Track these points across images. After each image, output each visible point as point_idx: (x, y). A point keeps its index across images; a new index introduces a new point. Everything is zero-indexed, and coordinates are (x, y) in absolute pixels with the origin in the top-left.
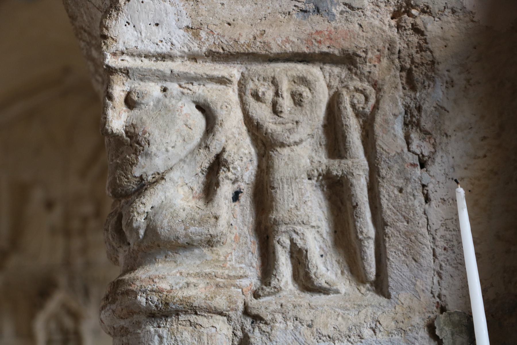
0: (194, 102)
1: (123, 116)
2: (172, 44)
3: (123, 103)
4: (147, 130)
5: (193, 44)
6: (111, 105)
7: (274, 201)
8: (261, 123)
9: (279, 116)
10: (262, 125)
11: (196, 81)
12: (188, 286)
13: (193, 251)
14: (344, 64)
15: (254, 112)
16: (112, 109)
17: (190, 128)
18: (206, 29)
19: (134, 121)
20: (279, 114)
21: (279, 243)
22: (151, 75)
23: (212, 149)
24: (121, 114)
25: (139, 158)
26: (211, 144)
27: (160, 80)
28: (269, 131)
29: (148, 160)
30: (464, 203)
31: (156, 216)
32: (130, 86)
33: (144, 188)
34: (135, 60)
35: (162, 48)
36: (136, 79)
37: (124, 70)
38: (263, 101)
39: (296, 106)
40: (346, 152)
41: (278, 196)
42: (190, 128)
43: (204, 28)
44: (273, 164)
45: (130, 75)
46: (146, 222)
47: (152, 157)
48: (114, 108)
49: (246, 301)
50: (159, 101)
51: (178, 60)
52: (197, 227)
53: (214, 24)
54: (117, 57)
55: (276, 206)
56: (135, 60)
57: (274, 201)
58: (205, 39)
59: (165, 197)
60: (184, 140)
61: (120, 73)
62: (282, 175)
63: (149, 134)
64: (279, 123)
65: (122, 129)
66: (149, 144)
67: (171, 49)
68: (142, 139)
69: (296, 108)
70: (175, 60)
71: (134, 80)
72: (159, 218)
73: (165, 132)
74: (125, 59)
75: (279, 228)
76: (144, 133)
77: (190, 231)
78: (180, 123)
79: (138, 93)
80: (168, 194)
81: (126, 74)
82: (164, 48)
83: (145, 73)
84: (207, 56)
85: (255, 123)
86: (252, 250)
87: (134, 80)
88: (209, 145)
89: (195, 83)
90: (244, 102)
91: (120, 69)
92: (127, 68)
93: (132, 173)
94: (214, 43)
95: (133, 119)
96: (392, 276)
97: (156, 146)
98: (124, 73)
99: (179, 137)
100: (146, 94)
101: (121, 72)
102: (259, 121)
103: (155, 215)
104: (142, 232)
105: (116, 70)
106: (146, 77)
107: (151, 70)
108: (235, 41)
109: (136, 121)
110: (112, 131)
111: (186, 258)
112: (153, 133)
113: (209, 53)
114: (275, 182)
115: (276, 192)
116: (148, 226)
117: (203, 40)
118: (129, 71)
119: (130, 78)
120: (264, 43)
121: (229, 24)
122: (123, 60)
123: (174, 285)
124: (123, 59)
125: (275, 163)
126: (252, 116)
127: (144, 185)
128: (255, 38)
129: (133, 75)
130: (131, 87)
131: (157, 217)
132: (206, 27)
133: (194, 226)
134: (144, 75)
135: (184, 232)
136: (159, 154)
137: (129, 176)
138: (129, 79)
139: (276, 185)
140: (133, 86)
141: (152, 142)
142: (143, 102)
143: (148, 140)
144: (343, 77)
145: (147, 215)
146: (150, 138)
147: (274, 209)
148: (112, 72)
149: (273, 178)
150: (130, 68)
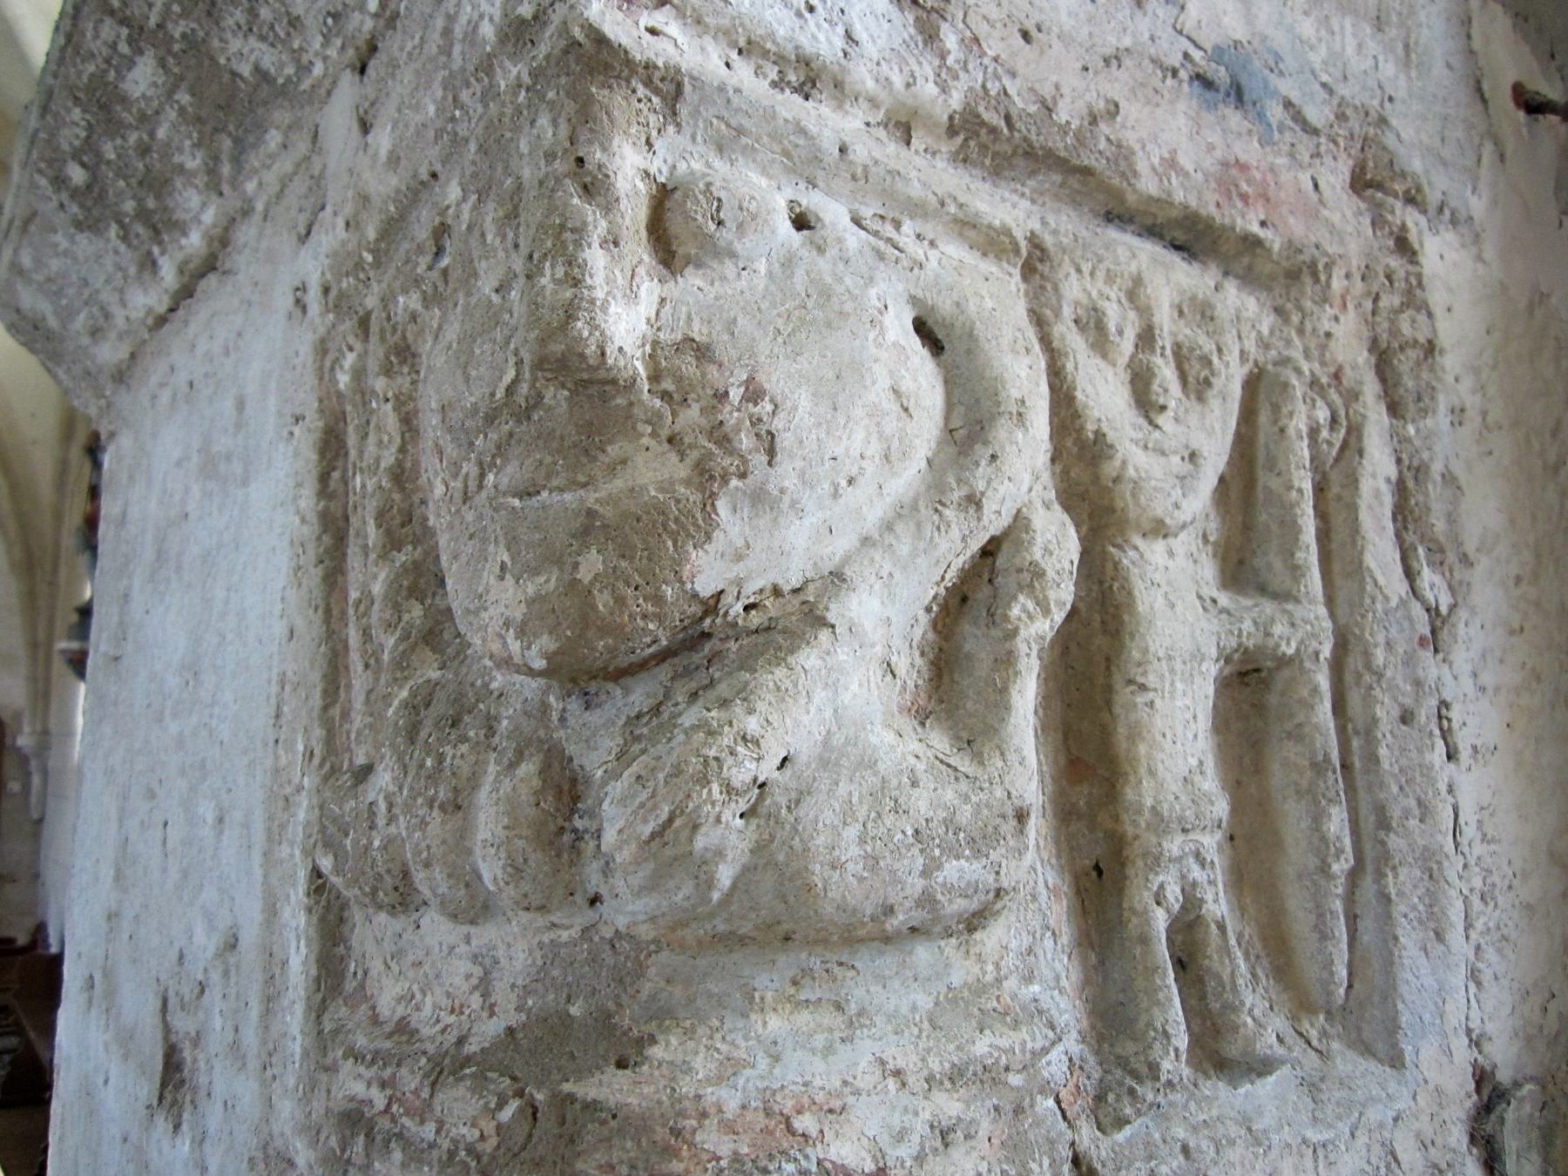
0: (914, 300)
1: (643, 293)
2: (849, 36)
3: (644, 234)
4: (767, 386)
5: (920, 63)
6: (603, 224)
7: (1143, 739)
8: (1111, 437)
9: (1151, 422)
10: (1111, 447)
11: (911, 219)
12: (946, 1145)
13: (911, 953)
14: (1269, 289)
15: (1089, 389)
16: (603, 244)
17: (906, 410)
18: (961, 26)
19: (696, 325)
20: (1152, 415)
21: (1158, 903)
22: (765, 139)
23: (989, 506)
24: (637, 279)
25: (722, 506)
26: (989, 493)
27: (790, 171)
28: (1131, 472)
29: (762, 522)
30: (1035, 664)
31: (803, 805)
32: (670, 161)
33: (708, 647)
34: (703, 49)
35: (814, 37)
36: (699, 138)
37: (662, 80)
38: (1110, 356)
39: (1188, 397)
40: (1298, 583)
41: (1159, 722)
42: (906, 410)
43: (953, 16)
44: (1130, 594)
45: (684, 110)
46: (753, 827)
47: (780, 511)
48: (616, 244)
49: (1081, 1149)
50: (789, 262)
51: (855, 110)
52: (968, 858)
53: (984, 17)
54: (633, 8)
55: (1149, 757)
56: (703, 49)
57: (1143, 739)
58: (957, 61)
59: (836, 711)
60: (887, 457)
61: (642, 91)
62: (1167, 642)
63: (772, 401)
64: (1154, 450)
65: (639, 354)
66: (771, 452)
67: (845, 54)
68: (740, 421)
69: (1188, 404)
70: (847, 106)
71: (694, 138)
72: (821, 813)
73: (835, 409)
74: (667, 30)
75: (1165, 844)
76: (754, 394)
77: (940, 880)
78: (878, 393)
79: (719, 200)
80: (846, 698)
81: (664, 99)
82: (821, 37)
83: (746, 123)
84: (952, 131)
85: (1091, 435)
86: (1052, 923)
87: (694, 138)
88: (983, 494)
89: (908, 227)
90: (1055, 344)
91: (649, 66)
92: (678, 70)
93: (686, 574)
94: (984, 86)
95: (689, 317)
96: (1406, 996)
97: (799, 464)
98: (657, 91)
99: (874, 438)
100: (754, 217)
101: (648, 83)
102: (1105, 428)
103: (798, 802)
104: (725, 875)
105: (629, 62)
106: (744, 140)
107: (774, 116)
108: (1043, 102)
109: (705, 331)
110: (603, 354)
111: (879, 988)
112: (789, 404)
113: (967, 121)
114: (1150, 668)
115: (1151, 704)
116: (759, 849)
117: (950, 61)
118: (687, 88)
119: (678, 125)
120: (1119, 146)
121: (1026, 35)
122: (653, 32)
123: (884, 1141)
124: (659, 26)
125: (1136, 593)
126: (1086, 406)
127: (706, 636)
128: (1094, 121)
129: (695, 113)
130: (674, 167)
131: (806, 811)
132: (960, 15)
133: (957, 858)
134: (740, 131)
135: (920, 884)
136: (808, 502)
137: (668, 591)
138: (671, 129)
139: (1151, 680)
140: (682, 167)
141: (785, 441)
142: (738, 246)
143: (769, 433)
144: (1265, 331)
145: (761, 797)
146: (778, 424)
147: (1143, 771)
148: (608, 67)
149: (1145, 651)
150: (693, 78)
